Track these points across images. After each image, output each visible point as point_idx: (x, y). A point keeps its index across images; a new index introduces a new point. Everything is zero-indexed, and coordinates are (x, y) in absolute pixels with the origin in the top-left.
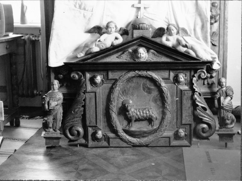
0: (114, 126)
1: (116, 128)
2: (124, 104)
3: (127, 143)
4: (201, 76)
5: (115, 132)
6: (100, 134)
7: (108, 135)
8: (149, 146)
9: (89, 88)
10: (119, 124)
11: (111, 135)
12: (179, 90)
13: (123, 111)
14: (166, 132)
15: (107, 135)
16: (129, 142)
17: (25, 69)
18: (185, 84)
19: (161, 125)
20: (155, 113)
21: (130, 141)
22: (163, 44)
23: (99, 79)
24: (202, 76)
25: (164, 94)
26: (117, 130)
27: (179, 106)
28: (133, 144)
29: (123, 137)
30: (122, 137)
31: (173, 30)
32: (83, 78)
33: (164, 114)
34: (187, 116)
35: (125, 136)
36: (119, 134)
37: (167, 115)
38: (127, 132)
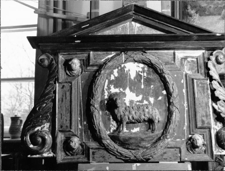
0: (97, 129)
1: (100, 133)
2: (111, 98)
3: (116, 156)
4: (219, 58)
5: (98, 139)
6: (75, 143)
7: (88, 144)
8: (149, 161)
9: (62, 74)
10: (106, 128)
11: (93, 145)
12: (189, 79)
13: (111, 105)
14: (120, 11)
15: (86, 145)
16: (119, 154)
17: (115, 154)
18: (204, 152)
19: (166, 129)
20: (159, 116)
21: (120, 153)
22: (163, 14)
23: (76, 64)
24: (221, 58)
25: (168, 84)
26: (100, 136)
27: (190, 97)
28: (126, 157)
29: (110, 147)
30: (108, 146)
31: (198, 139)
32: (54, 62)
33: (170, 113)
34: (203, 116)
35: (112, 146)
36: (104, 142)
37: (174, 113)
38: (114, 138)
